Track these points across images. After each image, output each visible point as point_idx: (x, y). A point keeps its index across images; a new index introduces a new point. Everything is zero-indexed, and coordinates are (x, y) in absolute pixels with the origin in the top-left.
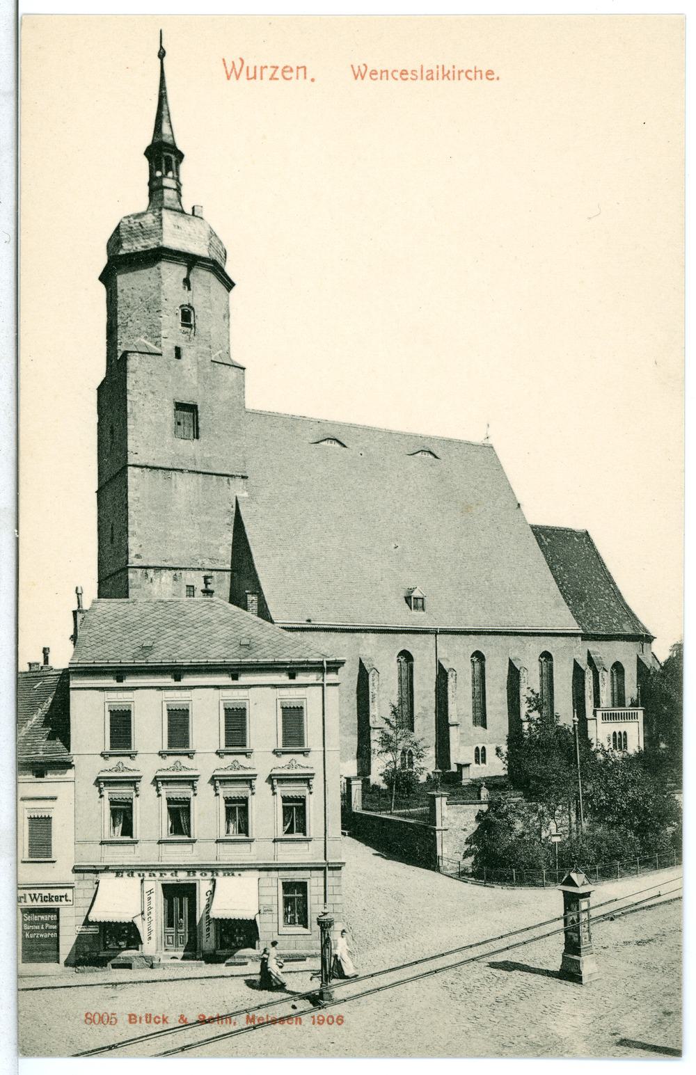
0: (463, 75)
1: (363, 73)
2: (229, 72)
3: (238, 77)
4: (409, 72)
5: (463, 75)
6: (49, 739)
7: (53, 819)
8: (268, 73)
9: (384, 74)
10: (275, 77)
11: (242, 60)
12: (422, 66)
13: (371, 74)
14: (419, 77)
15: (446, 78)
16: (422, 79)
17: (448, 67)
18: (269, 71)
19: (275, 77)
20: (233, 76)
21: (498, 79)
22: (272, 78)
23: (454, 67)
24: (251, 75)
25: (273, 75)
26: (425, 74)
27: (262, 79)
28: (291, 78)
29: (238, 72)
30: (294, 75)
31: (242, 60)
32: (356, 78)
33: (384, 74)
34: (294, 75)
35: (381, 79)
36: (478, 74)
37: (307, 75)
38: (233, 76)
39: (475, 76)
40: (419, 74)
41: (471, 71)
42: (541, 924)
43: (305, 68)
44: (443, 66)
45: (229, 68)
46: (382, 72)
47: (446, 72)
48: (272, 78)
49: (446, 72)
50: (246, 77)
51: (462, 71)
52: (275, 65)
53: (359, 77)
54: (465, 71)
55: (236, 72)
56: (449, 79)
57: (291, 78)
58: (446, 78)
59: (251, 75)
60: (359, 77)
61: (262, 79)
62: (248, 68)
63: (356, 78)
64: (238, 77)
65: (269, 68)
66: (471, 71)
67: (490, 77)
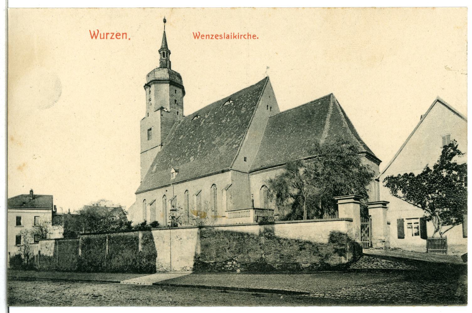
0: (242, 37)
1: (198, 36)
2: (92, 35)
3: (96, 38)
4: (219, 36)
5: (242, 37)
6: (105, 206)
7: (334, 94)
8: (109, 36)
9: (208, 37)
10: (113, 38)
11: (98, 31)
12: (224, 33)
13: (202, 36)
14: (223, 37)
15: (235, 38)
16: (224, 38)
17: (236, 34)
18: (111, 35)
19: (113, 38)
20: (94, 37)
21: (258, 38)
22: (111, 38)
23: (238, 33)
24: (102, 37)
25: (112, 37)
26: (226, 36)
27: (107, 38)
28: (120, 38)
29: (198, 36)
30: (121, 37)
31: (98, 31)
32: (92, 38)
33: (208, 37)
34: (121, 37)
35: (206, 38)
36: (249, 37)
37: (127, 37)
38: (94, 37)
39: (248, 37)
40: (223, 36)
41: (246, 35)
42: (254, 225)
43: (126, 34)
44: (234, 33)
45: (195, 35)
46: (123, 34)
47: (235, 36)
48: (111, 38)
49: (235, 36)
50: (99, 37)
51: (242, 35)
52: (113, 32)
53: (196, 37)
54: (243, 35)
55: (197, 36)
56: (236, 38)
57: (120, 38)
58: (235, 38)
59: (102, 37)
60: (196, 37)
61: (107, 38)
62: (101, 34)
63: (92, 38)
64: (96, 38)
65: (110, 34)
66: (246, 35)
67: (254, 38)
